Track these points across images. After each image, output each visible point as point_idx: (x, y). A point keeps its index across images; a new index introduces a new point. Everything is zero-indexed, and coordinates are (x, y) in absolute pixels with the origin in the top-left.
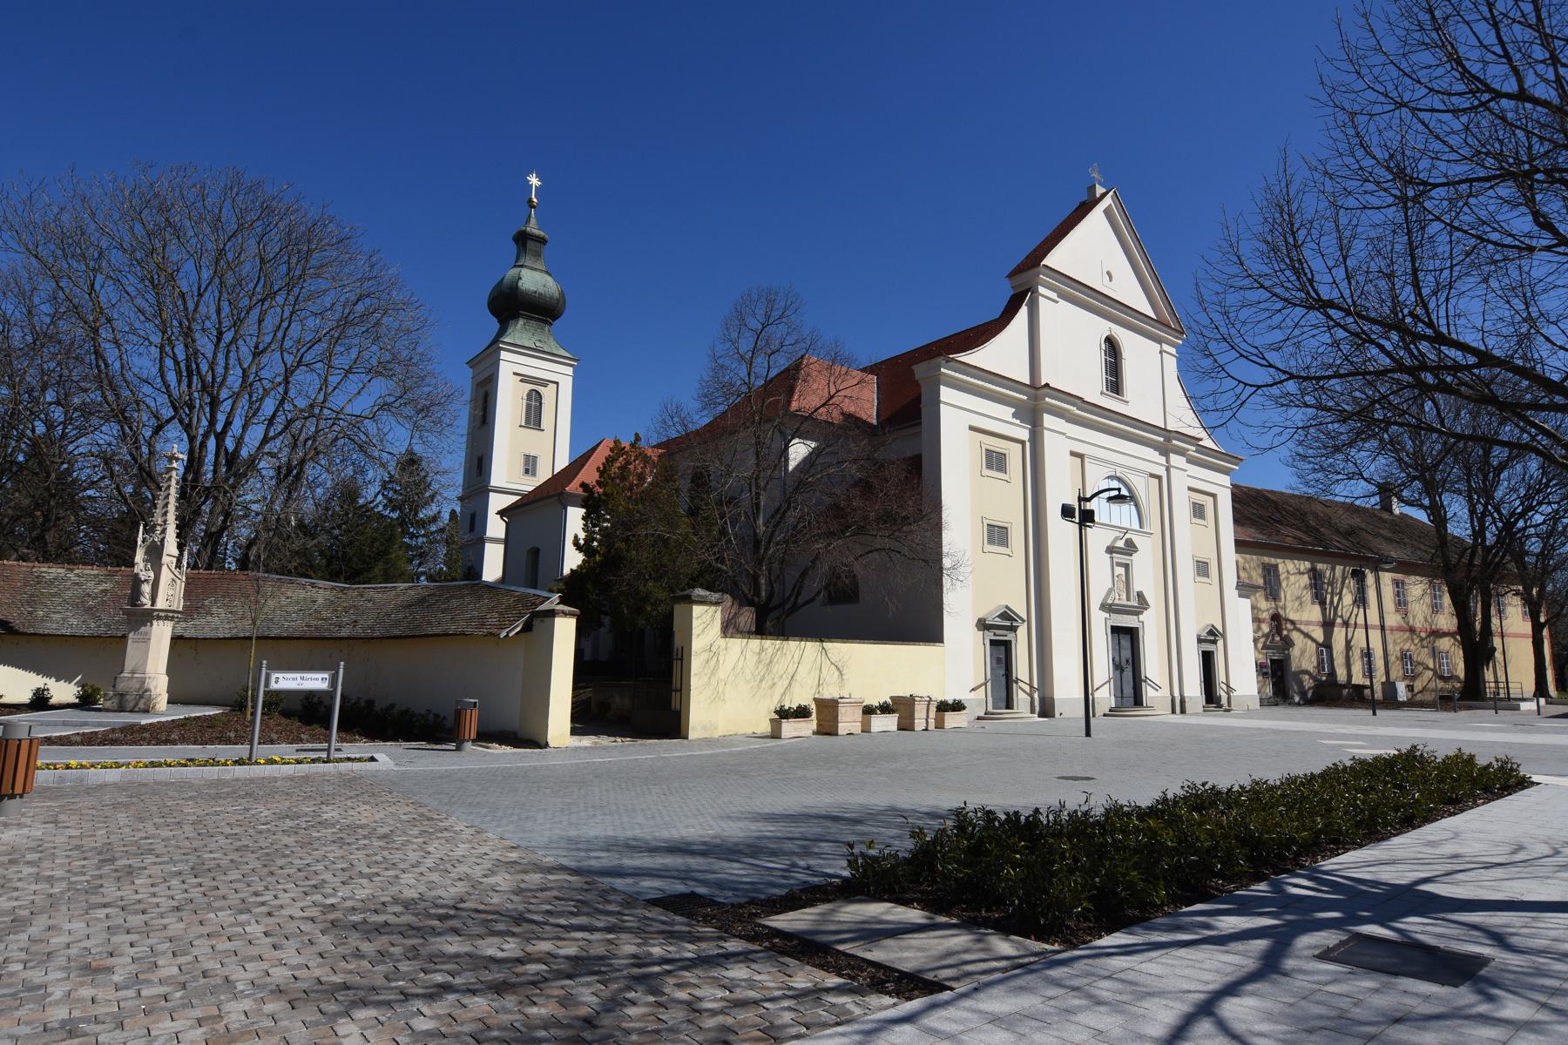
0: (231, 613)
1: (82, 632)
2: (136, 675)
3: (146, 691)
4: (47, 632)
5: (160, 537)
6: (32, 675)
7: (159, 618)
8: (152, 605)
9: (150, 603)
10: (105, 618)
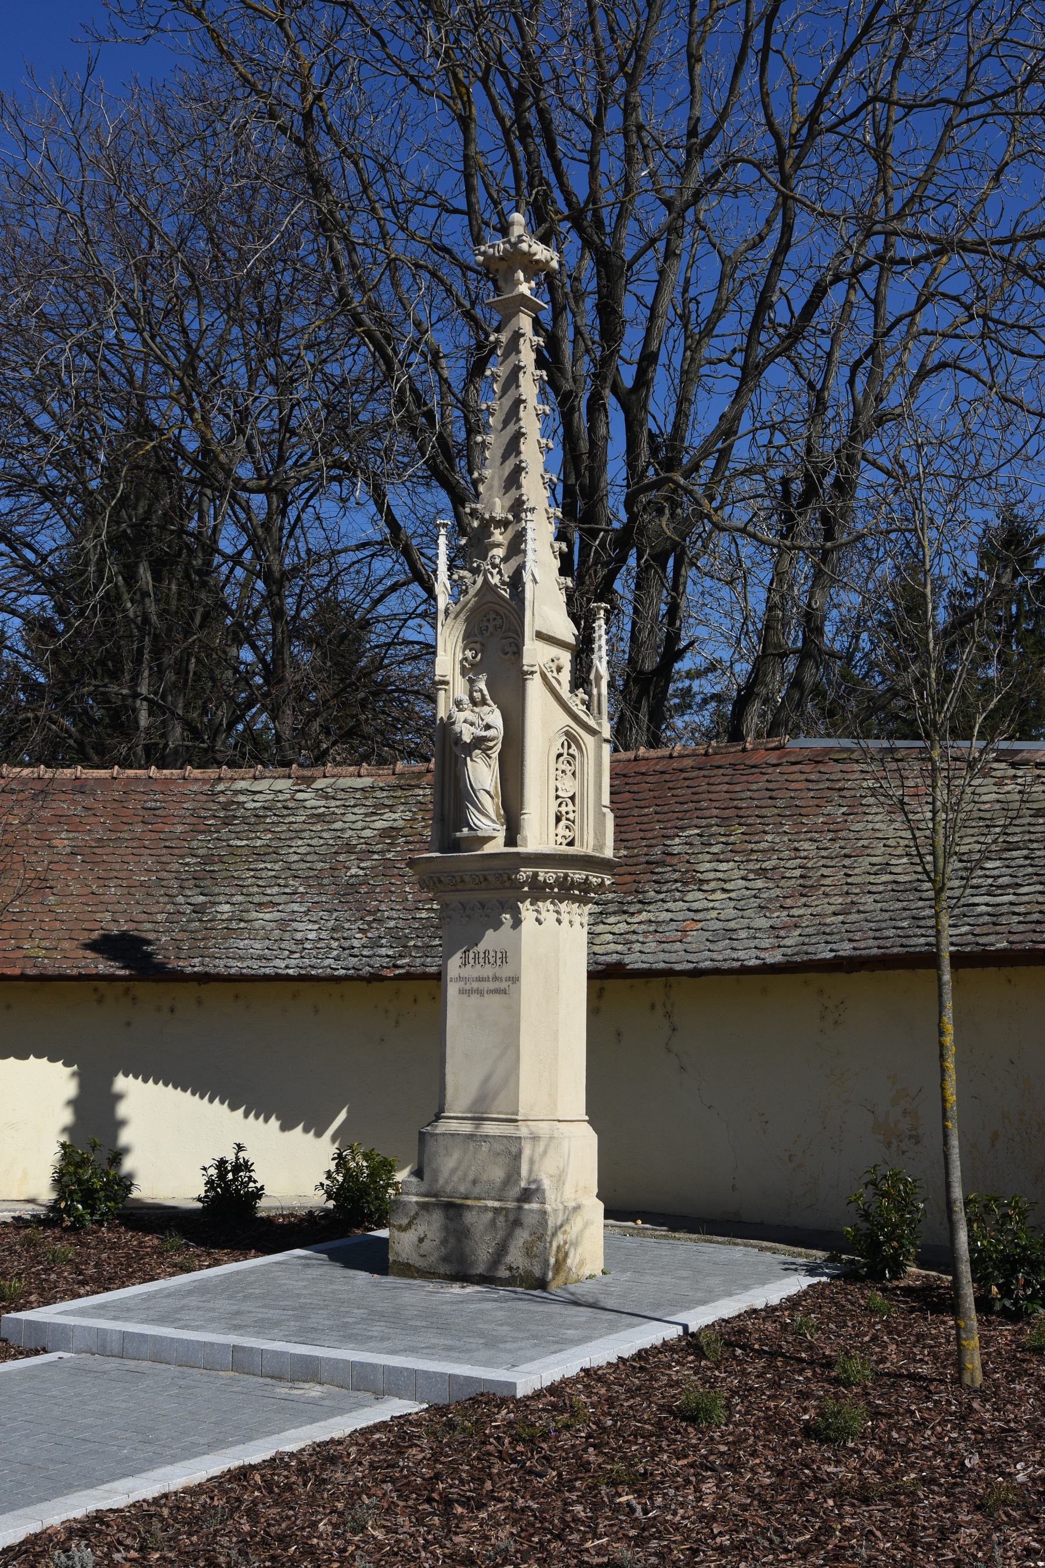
0: (762, 872)
1: (331, 964)
2: (490, 1129)
3: (527, 1195)
4: (236, 967)
5: (508, 570)
6: (219, 1109)
7: (538, 891)
8: (511, 840)
9: (501, 835)
10: (393, 916)
